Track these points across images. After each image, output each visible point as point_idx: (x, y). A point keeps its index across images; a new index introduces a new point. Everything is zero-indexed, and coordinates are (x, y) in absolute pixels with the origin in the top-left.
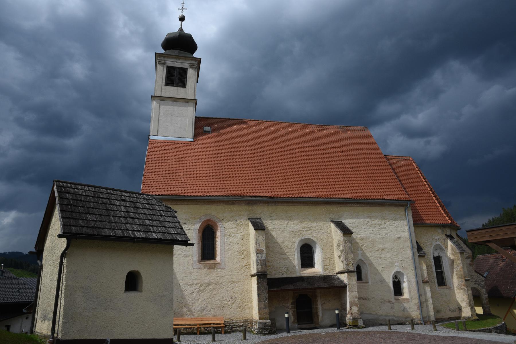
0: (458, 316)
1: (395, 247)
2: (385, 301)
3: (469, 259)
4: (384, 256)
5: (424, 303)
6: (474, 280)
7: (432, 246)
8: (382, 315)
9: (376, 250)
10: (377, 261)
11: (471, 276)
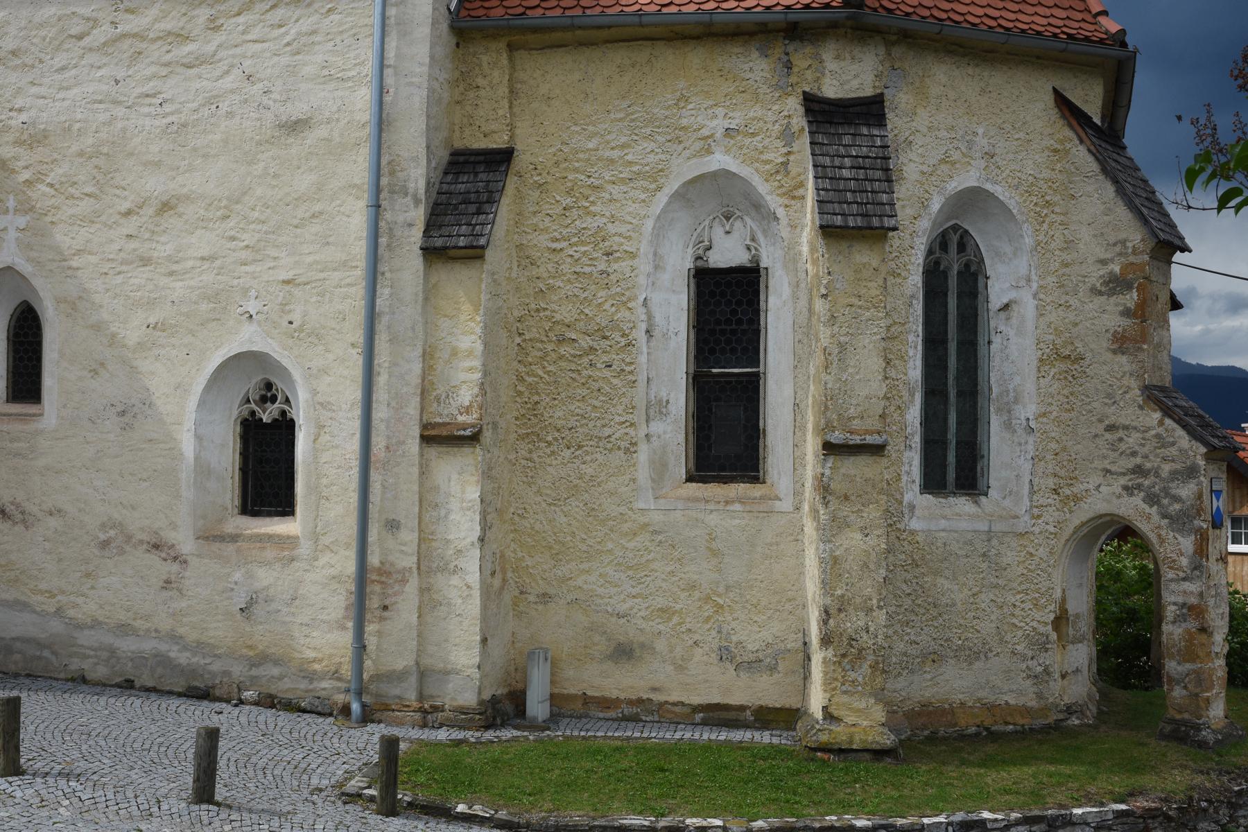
0: (792, 702)
1: (259, 192)
2: (129, 538)
3: (1121, 299)
4: (169, 249)
5: (404, 581)
6: (1131, 463)
7: (659, 189)
8: (96, 624)
9: (125, 206)
10: (119, 279)
11: (1111, 428)
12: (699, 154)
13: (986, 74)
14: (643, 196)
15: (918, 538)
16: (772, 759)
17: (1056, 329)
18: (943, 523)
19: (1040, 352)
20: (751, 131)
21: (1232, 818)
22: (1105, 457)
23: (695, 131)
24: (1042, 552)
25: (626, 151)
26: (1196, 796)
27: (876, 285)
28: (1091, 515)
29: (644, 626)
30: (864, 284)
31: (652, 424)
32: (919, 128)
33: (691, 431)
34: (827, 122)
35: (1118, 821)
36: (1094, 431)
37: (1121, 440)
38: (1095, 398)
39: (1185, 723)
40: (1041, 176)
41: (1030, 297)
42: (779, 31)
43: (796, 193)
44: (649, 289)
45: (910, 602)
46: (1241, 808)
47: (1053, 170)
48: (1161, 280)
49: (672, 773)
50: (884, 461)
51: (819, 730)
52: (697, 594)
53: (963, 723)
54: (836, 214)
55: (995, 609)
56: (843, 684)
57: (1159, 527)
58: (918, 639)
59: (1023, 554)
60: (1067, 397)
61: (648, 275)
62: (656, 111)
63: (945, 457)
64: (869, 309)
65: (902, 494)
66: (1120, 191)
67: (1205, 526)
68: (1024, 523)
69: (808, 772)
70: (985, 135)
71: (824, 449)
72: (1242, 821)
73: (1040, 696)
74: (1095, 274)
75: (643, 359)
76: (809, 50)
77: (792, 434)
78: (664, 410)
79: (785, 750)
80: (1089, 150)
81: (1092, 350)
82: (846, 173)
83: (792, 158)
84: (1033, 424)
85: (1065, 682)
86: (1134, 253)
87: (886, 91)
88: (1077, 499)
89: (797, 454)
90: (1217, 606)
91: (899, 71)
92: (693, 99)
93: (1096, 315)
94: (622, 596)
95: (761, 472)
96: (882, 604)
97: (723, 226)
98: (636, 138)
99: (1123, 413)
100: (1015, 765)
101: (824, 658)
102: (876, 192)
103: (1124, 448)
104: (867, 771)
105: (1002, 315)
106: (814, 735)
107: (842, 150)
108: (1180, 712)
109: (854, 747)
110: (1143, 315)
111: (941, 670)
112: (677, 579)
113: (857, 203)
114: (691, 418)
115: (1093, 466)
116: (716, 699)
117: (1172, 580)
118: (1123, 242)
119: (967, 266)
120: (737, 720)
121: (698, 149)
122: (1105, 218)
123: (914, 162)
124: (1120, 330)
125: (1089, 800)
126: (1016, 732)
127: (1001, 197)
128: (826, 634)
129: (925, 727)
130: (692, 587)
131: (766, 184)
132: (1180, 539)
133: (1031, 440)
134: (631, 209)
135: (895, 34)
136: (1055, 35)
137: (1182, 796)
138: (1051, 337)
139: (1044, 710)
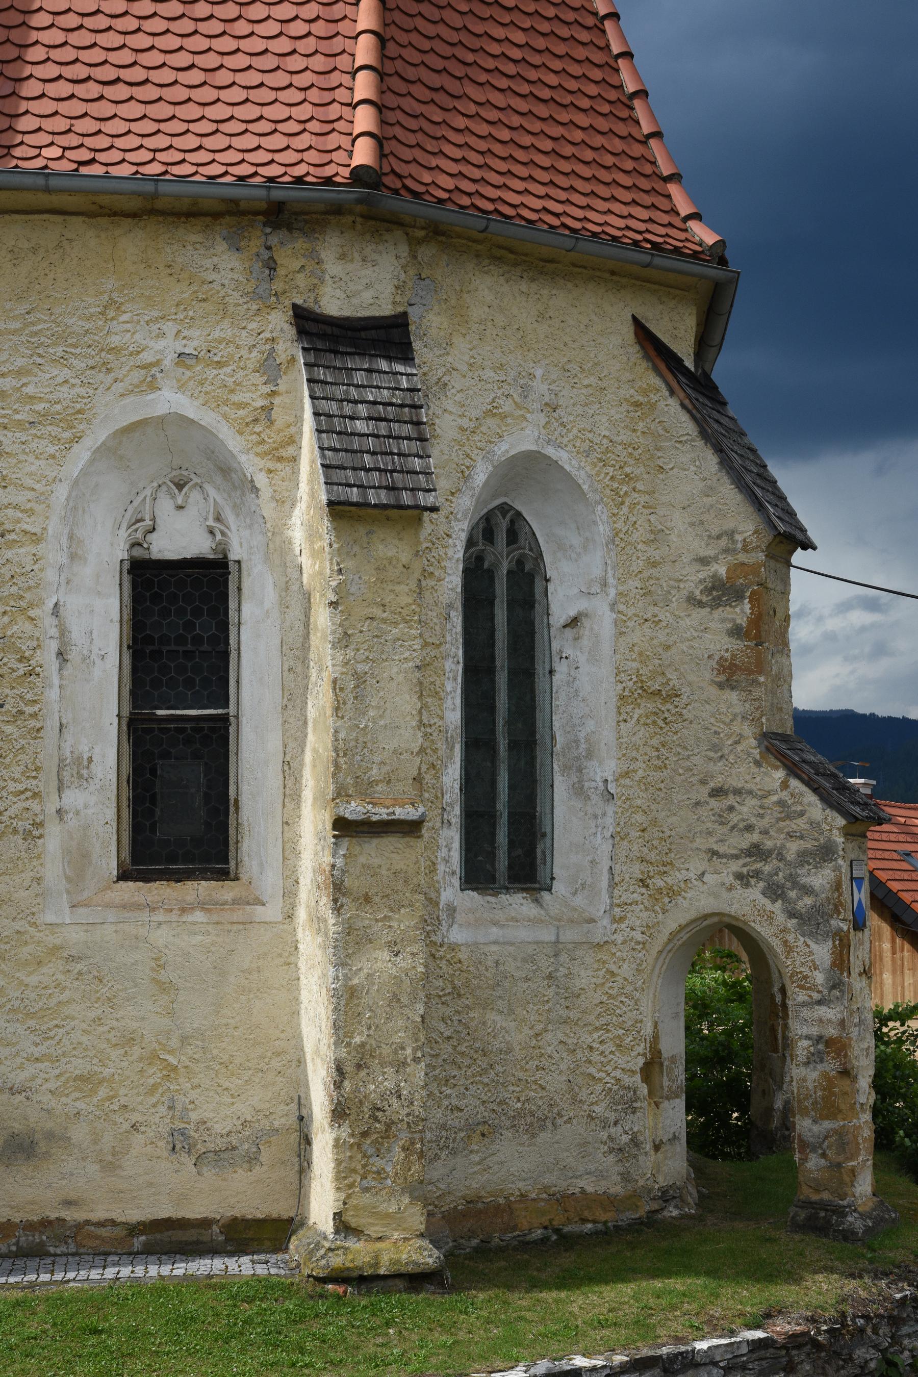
0: (281, 1209)
6: (747, 841)
7: (77, 439)
11: (717, 793)
12: (137, 389)
13: (545, 292)
14: (52, 450)
15: (461, 956)
16: (261, 1300)
17: (640, 654)
18: (495, 932)
19: (620, 686)
20: (216, 359)
21: (895, 1339)
22: (710, 834)
23: (131, 354)
24: (626, 970)
25: (24, 380)
26: (851, 1311)
27: (406, 589)
28: (692, 915)
29: (53, 1103)
30: (391, 587)
31: (67, 793)
32: (457, 365)
33: (125, 803)
34: (331, 351)
35: (754, 1356)
36: (694, 796)
37: (731, 808)
38: (696, 751)
39: (823, 1206)
40: (619, 439)
41: (606, 608)
42: (257, 213)
43: (284, 453)
44: (62, 589)
45: (450, 1049)
46: (904, 1325)
47: (634, 431)
48: (780, 588)
49: (110, 1335)
50: (420, 845)
51: (330, 1249)
52: (136, 1051)
53: (525, 1225)
54: (350, 486)
55: (565, 1054)
56: (364, 1177)
57: (785, 930)
58: (461, 1104)
59: (601, 973)
60: (657, 750)
61: (61, 568)
62: (70, 321)
63: (493, 835)
64: (397, 623)
65: (438, 891)
66: (725, 463)
67: (845, 928)
68: (603, 928)
69: (317, 1316)
70: (544, 378)
71: (334, 828)
72: (906, 1342)
73: (626, 1177)
74: (693, 578)
75: (53, 694)
76: (301, 243)
77: (280, 806)
78: (85, 772)
79: (280, 1284)
80: (683, 406)
81: (690, 684)
82: (360, 426)
83: (277, 401)
84: (612, 788)
85: (660, 1155)
86: (745, 549)
87: (410, 310)
88: (673, 893)
89: (287, 835)
90: (861, 1039)
91: (427, 282)
92: (128, 306)
93: (695, 634)
94: (19, 1060)
95: (232, 864)
96: (419, 1054)
97: (173, 497)
98: (39, 360)
99: (734, 771)
100: (607, 1283)
101: (337, 1140)
102: (405, 455)
103: (735, 820)
104: (403, 1308)
105: (569, 632)
106: (322, 1257)
107: (354, 393)
108: (817, 1191)
109: (382, 1271)
110: (758, 636)
111: (494, 1147)
112: (106, 1028)
113: (378, 469)
114: (125, 784)
115: (694, 845)
116: (166, 1211)
117: (803, 1004)
118: (731, 534)
119: (520, 562)
120: (198, 1242)
121: (136, 381)
122: (705, 499)
123: (451, 413)
124: (728, 655)
125: (713, 1327)
126: (597, 1233)
127: (567, 467)
128: (339, 1103)
129: (472, 1234)
130: (129, 1040)
131: (238, 437)
132: (813, 946)
133: (610, 810)
134: (33, 468)
135: (423, 228)
136: (636, 243)
137: (833, 1312)
138: (635, 665)
139: (633, 1198)
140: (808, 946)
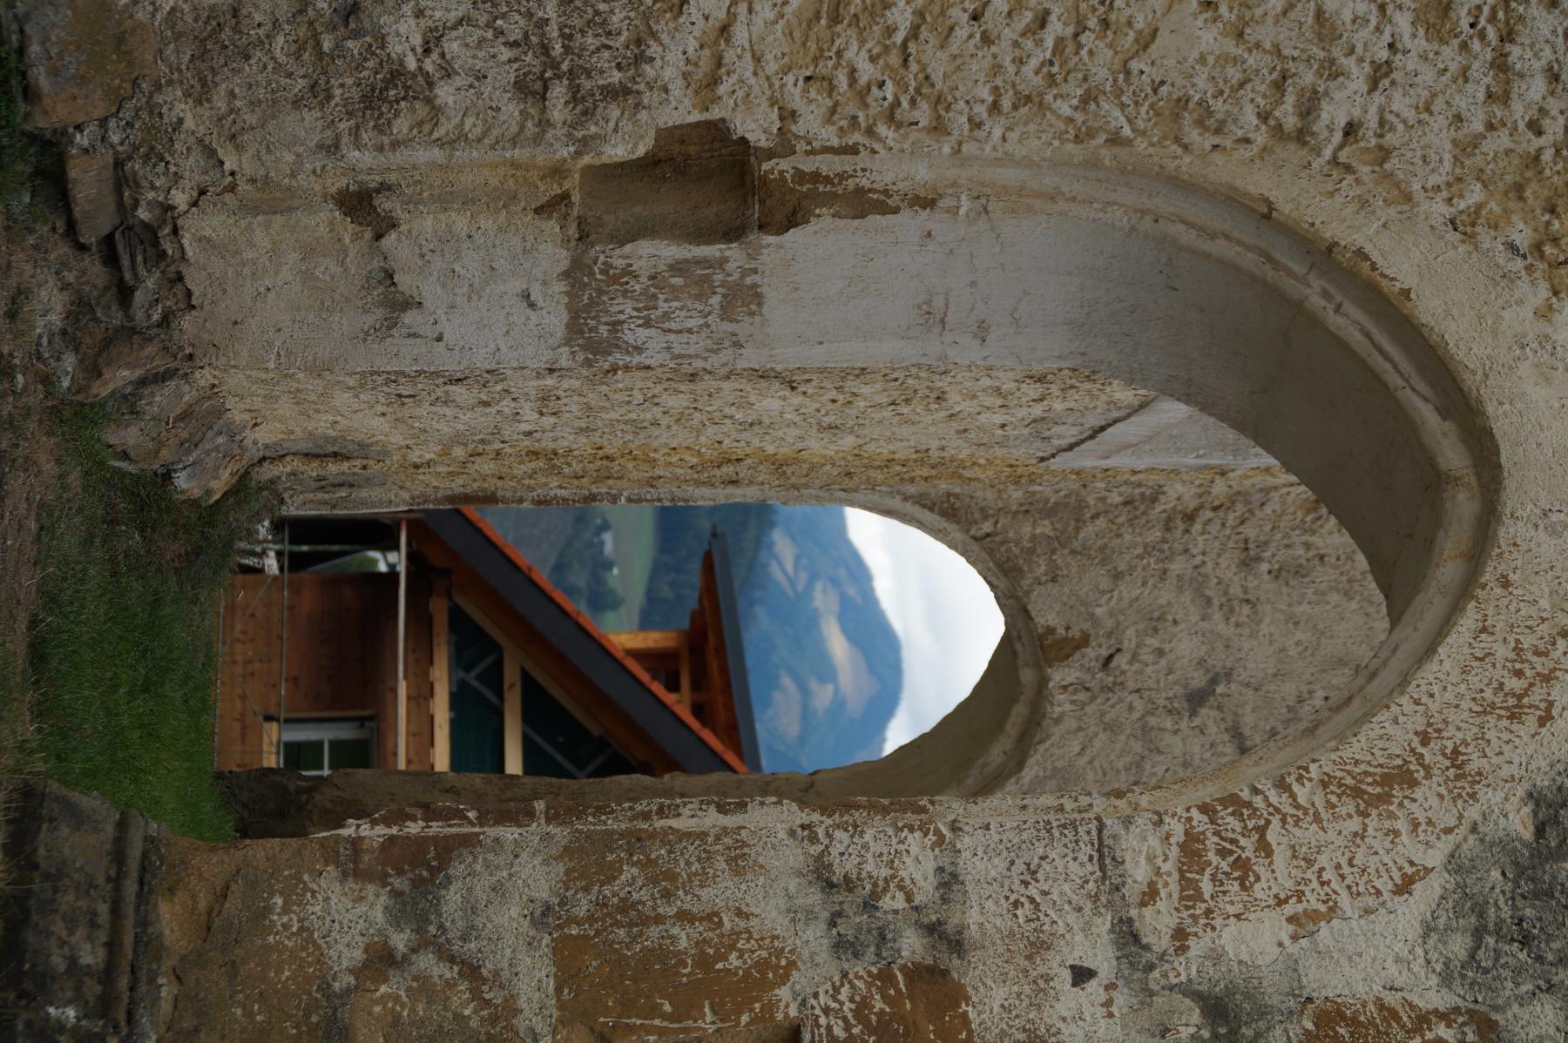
117: (1105, 855)
140: (1404, 887)
